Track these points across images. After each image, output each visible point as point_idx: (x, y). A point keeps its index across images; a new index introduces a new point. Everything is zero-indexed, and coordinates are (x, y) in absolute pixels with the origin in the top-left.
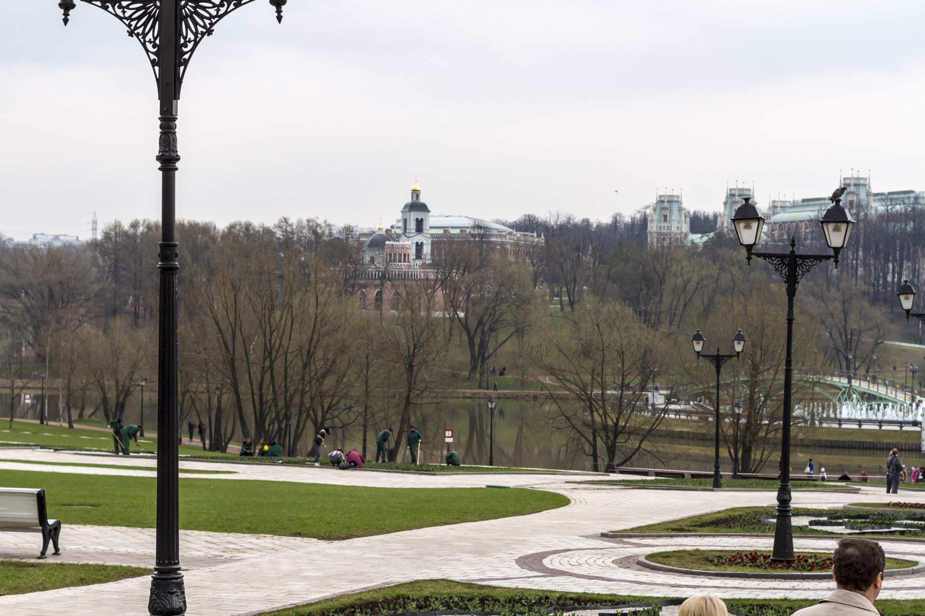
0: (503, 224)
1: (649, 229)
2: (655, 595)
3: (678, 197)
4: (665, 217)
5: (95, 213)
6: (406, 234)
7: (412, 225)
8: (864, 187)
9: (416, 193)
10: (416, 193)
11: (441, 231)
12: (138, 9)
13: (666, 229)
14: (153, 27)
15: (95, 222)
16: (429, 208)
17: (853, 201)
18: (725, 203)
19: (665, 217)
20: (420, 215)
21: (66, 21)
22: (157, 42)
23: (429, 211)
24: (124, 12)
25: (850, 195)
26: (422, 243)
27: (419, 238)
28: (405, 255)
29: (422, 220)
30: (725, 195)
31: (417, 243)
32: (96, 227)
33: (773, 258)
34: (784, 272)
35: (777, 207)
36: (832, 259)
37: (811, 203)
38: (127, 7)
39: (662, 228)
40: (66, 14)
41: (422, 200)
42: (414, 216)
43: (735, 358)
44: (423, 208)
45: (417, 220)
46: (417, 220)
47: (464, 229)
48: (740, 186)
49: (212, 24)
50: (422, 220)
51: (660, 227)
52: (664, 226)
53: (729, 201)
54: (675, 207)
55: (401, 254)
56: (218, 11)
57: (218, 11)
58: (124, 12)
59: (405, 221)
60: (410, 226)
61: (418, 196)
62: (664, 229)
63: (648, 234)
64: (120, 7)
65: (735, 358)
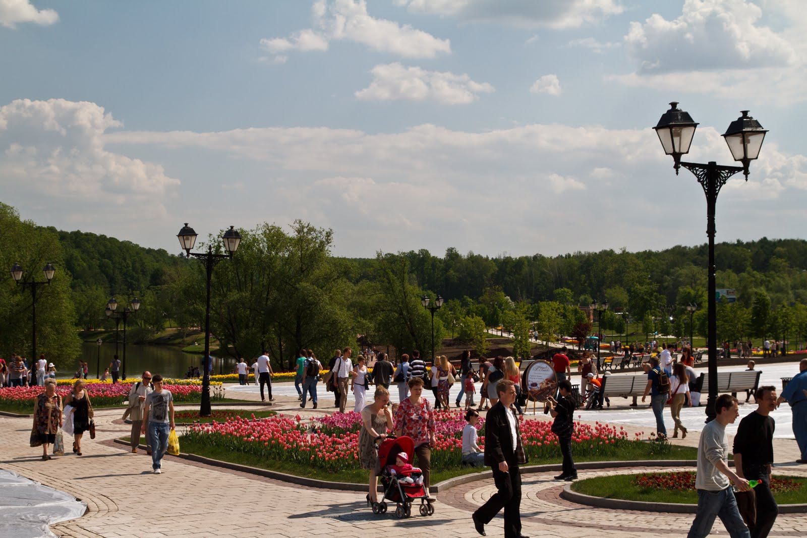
12: (701, 171)
14: (706, 180)
21: (677, 173)
22: (727, 171)
24: (696, 172)
33: (697, 168)
34: (705, 183)
36: (743, 171)
38: (698, 170)
40: (747, 177)
49: (726, 180)
56: (727, 175)
57: (727, 175)
58: (696, 172)
64: (695, 170)
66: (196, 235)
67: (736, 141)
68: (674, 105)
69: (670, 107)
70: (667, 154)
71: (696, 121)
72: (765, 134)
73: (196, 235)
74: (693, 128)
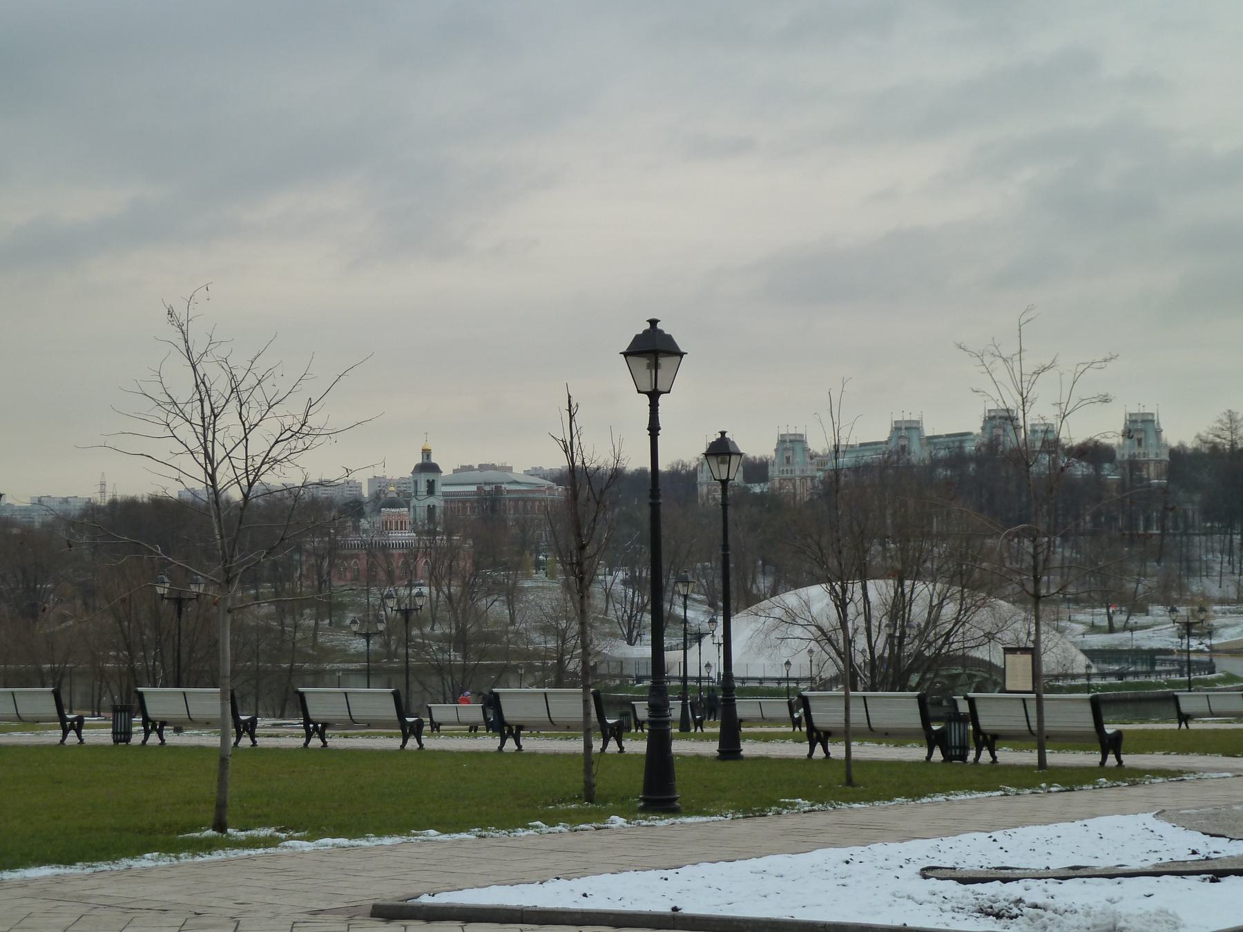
0: (544, 478)
1: (699, 480)
2: (328, 841)
3: (918, 422)
4: (788, 459)
5: (103, 473)
6: (417, 497)
7: (423, 488)
8: (739, 457)
9: (427, 453)
10: (427, 453)
11: (474, 488)
13: (789, 472)
15: (103, 484)
16: (441, 469)
17: (904, 446)
18: (776, 450)
19: (788, 459)
20: (431, 476)
23: (442, 472)
25: (901, 439)
26: (434, 506)
27: (432, 501)
28: (401, 522)
29: (433, 481)
30: (889, 429)
31: (429, 506)
32: (105, 489)
35: (1037, 431)
37: (868, 447)
39: (789, 472)
41: (434, 460)
42: (423, 478)
43: (195, 601)
44: (434, 468)
45: (428, 481)
46: (428, 481)
47: (499, 485)
48: (907, 418)
50: (433, 481)
51: (783, 470)
52: (787, 470)
53: (988, 425)
54: (798, 447)
55: (397, 522)
59: (416, 483)
60: (421, 488)
61: (428, 456)
62: (787, 473)
63: (698, 486)
65: (195, 601)
66: (681, 355)
67: (641, 363)
68: (653, 322)
69: (648, 326)
70: (639, 392)
71: (682, 350)
72: (682, 357)
73: (681, 355)
74: (679, 358)
